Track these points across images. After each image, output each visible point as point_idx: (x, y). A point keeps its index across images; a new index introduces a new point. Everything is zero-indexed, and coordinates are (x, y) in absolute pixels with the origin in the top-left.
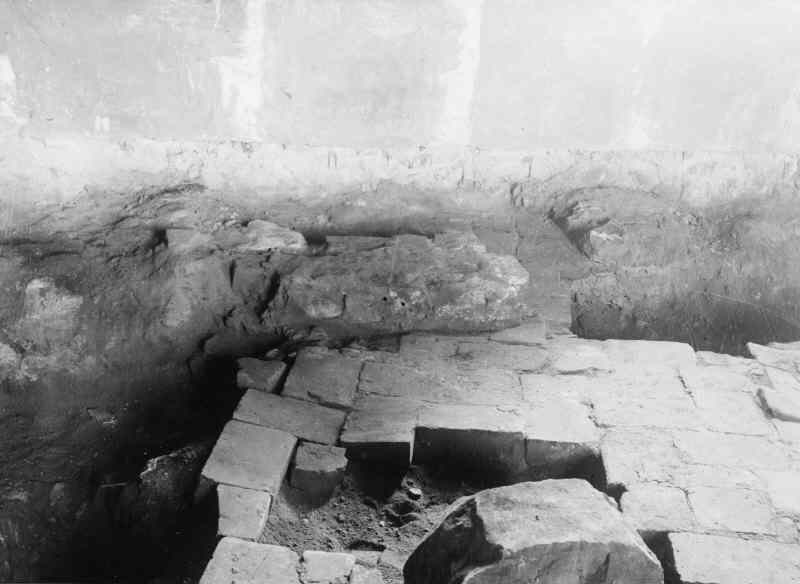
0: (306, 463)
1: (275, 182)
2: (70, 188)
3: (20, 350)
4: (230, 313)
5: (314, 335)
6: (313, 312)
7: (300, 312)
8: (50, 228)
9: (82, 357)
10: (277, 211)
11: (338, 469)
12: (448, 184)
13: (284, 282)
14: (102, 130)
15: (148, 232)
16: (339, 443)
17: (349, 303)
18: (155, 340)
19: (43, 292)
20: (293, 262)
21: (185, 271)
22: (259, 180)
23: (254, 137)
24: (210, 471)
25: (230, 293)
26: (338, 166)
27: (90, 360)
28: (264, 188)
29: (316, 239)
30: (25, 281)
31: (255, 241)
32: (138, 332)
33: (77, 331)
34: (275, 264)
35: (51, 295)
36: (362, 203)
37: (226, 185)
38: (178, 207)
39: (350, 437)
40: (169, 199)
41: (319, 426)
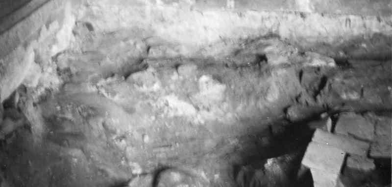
0: (351, 164)
1: (316, 34)
2: (212, 37)
3: (197, 108)
4: (300, 96)
5: (346, 108)
6: (344, 96)
7: (337, 96)
8: (205, 55)
9: (225, 113)
10: (322, 47)
11: (371, 169)
12: (15, 16)
13: (330, 80)
14: (231, 8)
15: (254, 56)
16: (369, 156)
17: (365, 93)
18: (261, 107)
19: (207, 83)
20: (332, 73)
21: (277, 73)
22: (308, 33)
23: (307, 10)
24: (306, 162)
25: (299, 86)
26: (351, 27)
27: (229, 115)
28: (310, 37)
29: (342, 64)
30: (199, 76)
31: (311, 61)
32: (252, 103)
33: (224, 101)
34: (323, 72)
35: (211, 83)
36: (364, 45)
37: (291, 35)
38: (267, 45)
39: (374, 154)
40: (262, 41)
41: (357, 149)
